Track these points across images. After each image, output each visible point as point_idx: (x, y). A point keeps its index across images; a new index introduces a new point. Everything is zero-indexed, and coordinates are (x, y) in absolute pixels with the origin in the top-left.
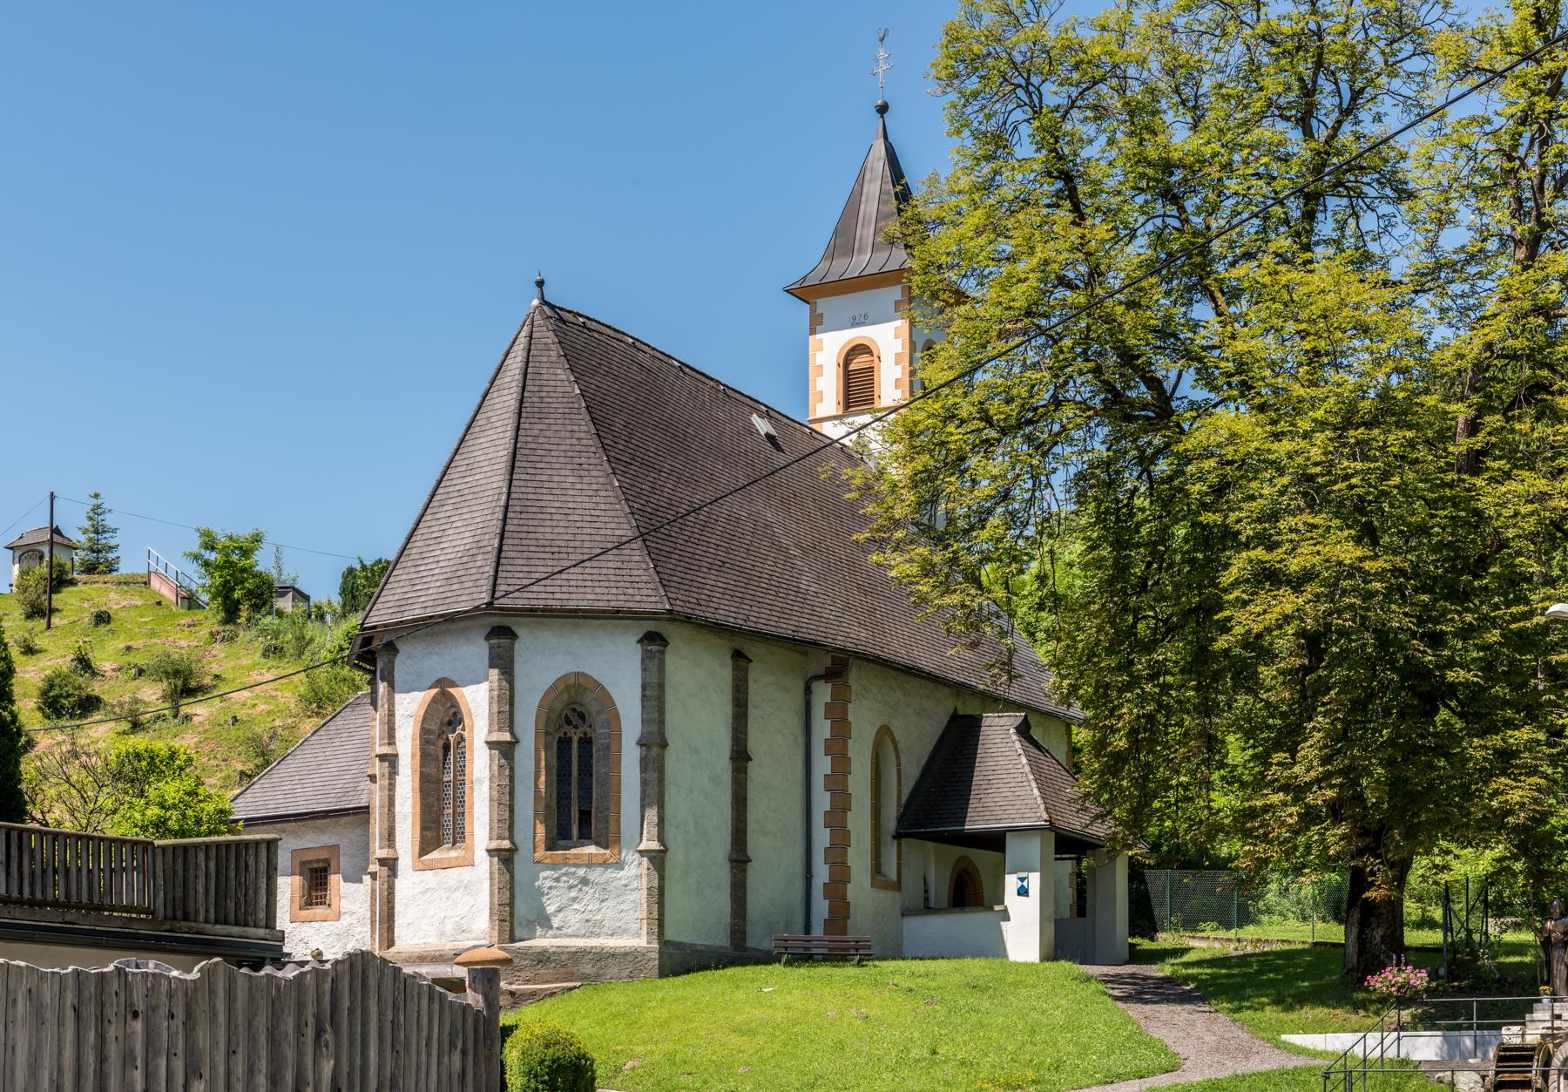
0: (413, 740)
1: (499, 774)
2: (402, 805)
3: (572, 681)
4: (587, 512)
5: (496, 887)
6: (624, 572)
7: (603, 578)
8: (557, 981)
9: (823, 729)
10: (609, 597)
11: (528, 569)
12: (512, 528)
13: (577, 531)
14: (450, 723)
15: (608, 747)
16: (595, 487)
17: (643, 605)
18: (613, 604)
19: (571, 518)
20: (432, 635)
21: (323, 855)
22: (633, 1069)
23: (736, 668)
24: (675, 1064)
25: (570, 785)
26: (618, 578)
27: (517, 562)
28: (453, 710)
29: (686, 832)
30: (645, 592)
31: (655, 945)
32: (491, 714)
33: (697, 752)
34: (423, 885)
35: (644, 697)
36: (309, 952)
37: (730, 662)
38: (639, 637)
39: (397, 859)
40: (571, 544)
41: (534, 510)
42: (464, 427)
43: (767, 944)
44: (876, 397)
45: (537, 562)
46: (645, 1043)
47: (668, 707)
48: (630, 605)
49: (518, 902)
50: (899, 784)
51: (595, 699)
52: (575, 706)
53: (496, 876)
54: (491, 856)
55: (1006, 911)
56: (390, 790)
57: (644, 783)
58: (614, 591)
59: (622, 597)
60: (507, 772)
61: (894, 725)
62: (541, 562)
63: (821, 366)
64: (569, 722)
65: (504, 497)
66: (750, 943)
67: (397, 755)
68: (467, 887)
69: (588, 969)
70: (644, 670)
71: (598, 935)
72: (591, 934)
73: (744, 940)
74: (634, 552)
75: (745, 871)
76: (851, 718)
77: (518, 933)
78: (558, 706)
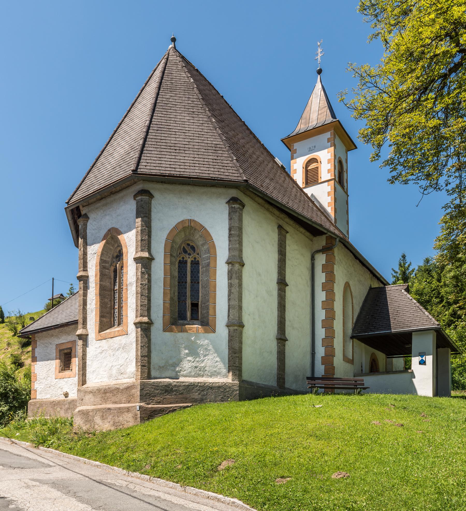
0: (96, 266)
1: (142, 277)
2: (90, 304)
3: (187, 225)
4: (197, 133)
5: (139, 346)
6: (218, 161)
7: (206, 163)
8: (177, 402)
9: (321, 278)
10: (209, 172)
11: (160, 156)
12: (152, 131)
13: (190, 140)
14: (117, 256)
15: (208, 265)
16: (201, 122)
17: (230, 177)
18: (211, 175)
19: (187, 134)
20: (106, 205)
21: (69, 346)
22: (228, 469)
23: (280, 234)
24: (266, 466)
25: (186, 288)
26: (215, 164)
27: (153, 152)
28: (119, 249)
29: (254, 319)
30: (231, 171)
31: (237, 382)
32: (137, 241)
33: (260, 275)
34: (101, 348)
35: (230, 235)
36: (62, 392)
37: (277, 230)
38: (227, 200)
39: (87, 335)
40: (187, 146)
41: (165, 129)
42: (131, 105)
43: (294, 387)
44: (319, 177)
45: (166, 153)
46: (237, 445)
47: (244, 244)
48: (222, 177)
49: (153, 355)
50: (353, 313)
51: (201, 236)
52: (189, 242)
53: (139, 339)
54: (137, 328)
55: (412, 372)
56: (84, 296)
57: (230, 286)
58: (212, 169)
59: (217, 173)
60: (146, 276)
61: (351, 283)
62: (169, 154)
63: (296, 170)
64: (185, 251)
65: (148, 122)
66: (287, 385)
67: (88, 277)
68: (124, 348)
69: (196, 396)
70: (230, 219)
71: (203, 376)
72: (199, 376)
73: (284, 383)
74: (224, 152)
75: (284, 345)
76: (335, 273)
77: (153, 374)
78: (179, 240)
